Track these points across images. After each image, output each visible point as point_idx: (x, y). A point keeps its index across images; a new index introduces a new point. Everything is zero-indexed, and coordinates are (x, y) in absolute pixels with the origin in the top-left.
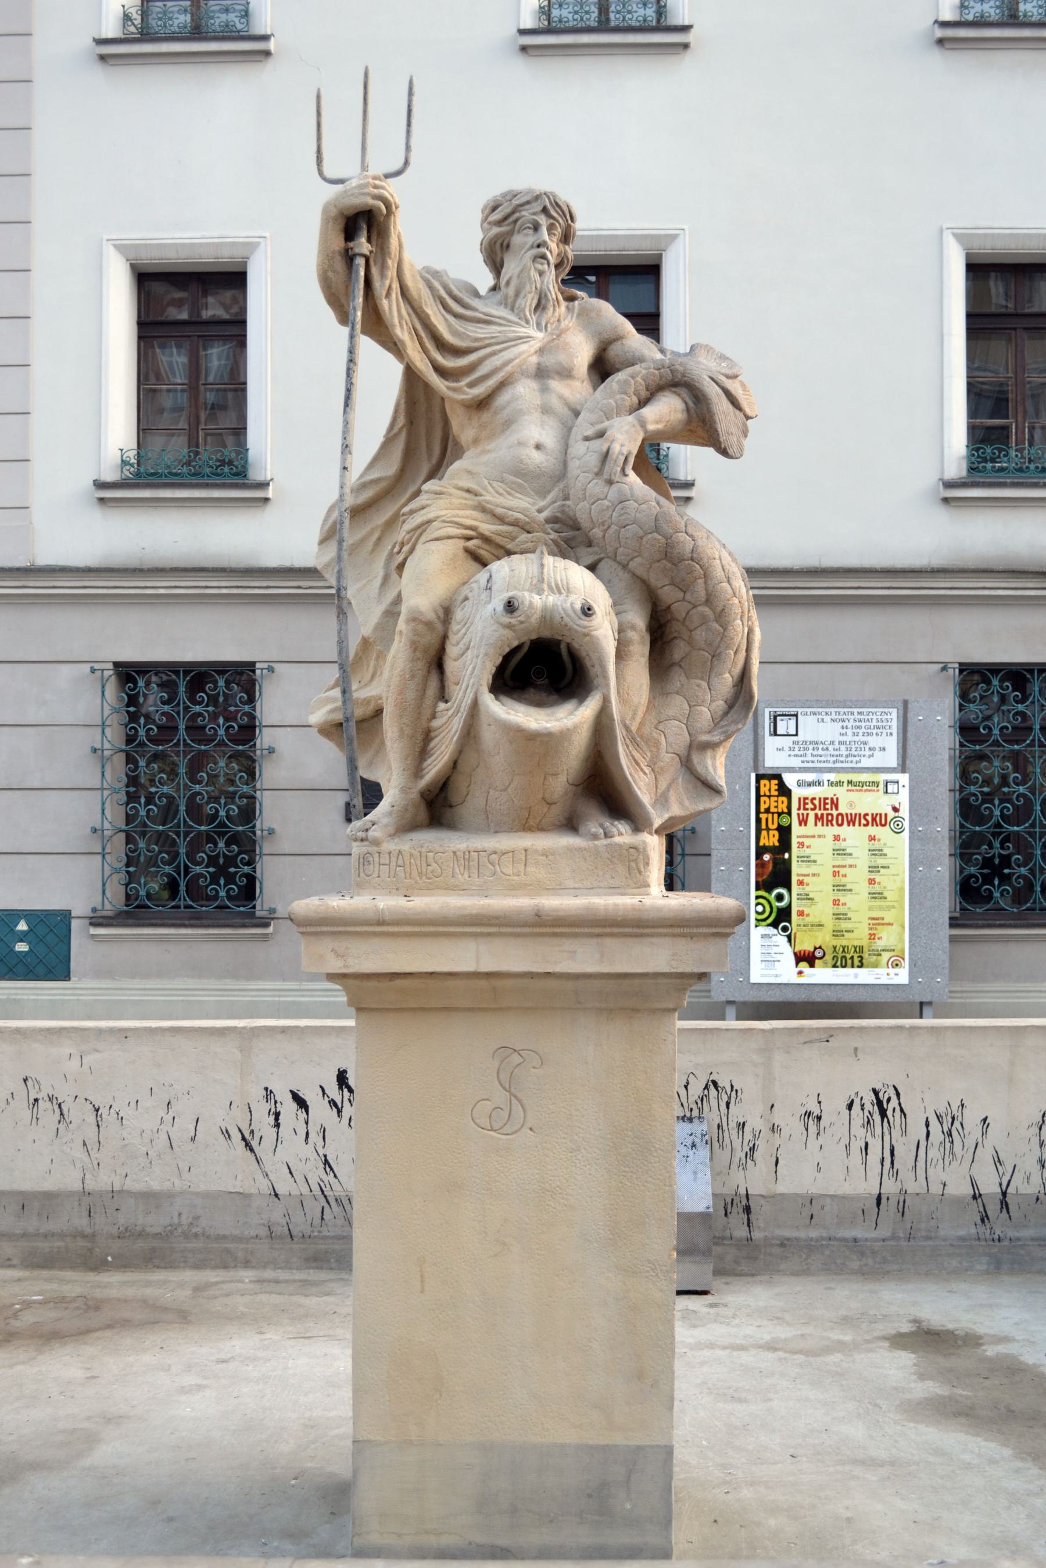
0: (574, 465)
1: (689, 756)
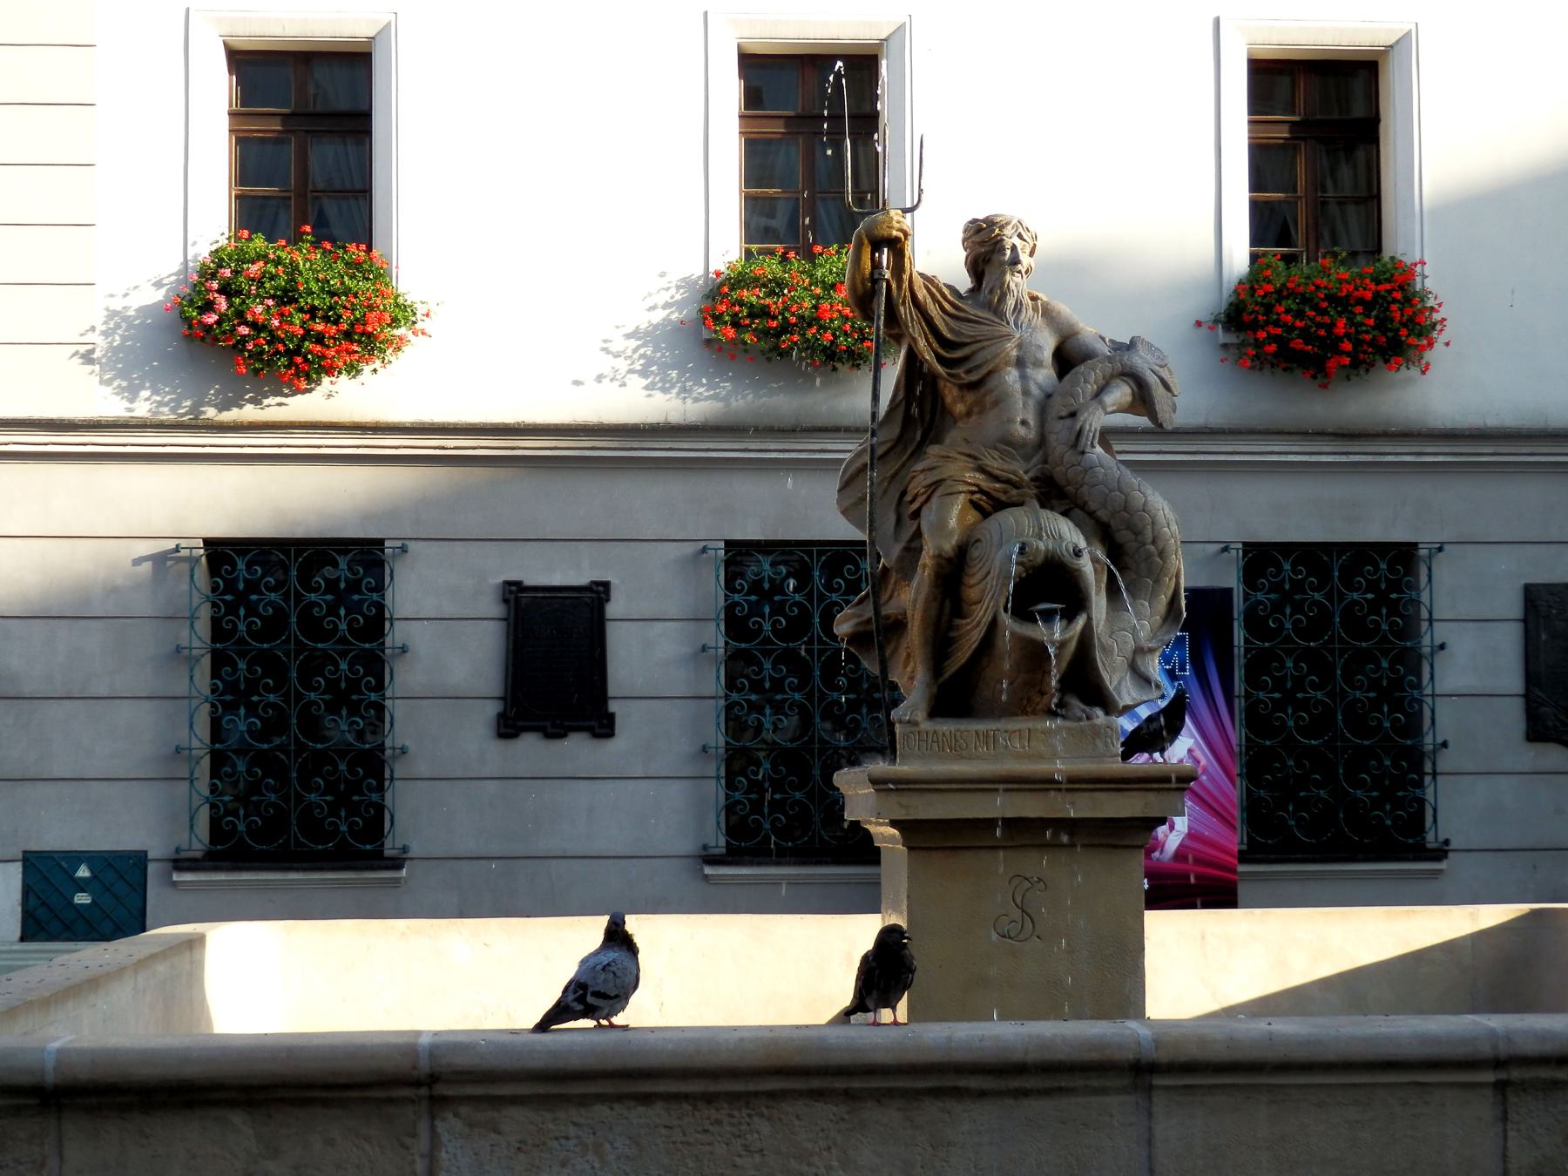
0: (1052, 438)
1: (1134, 660)
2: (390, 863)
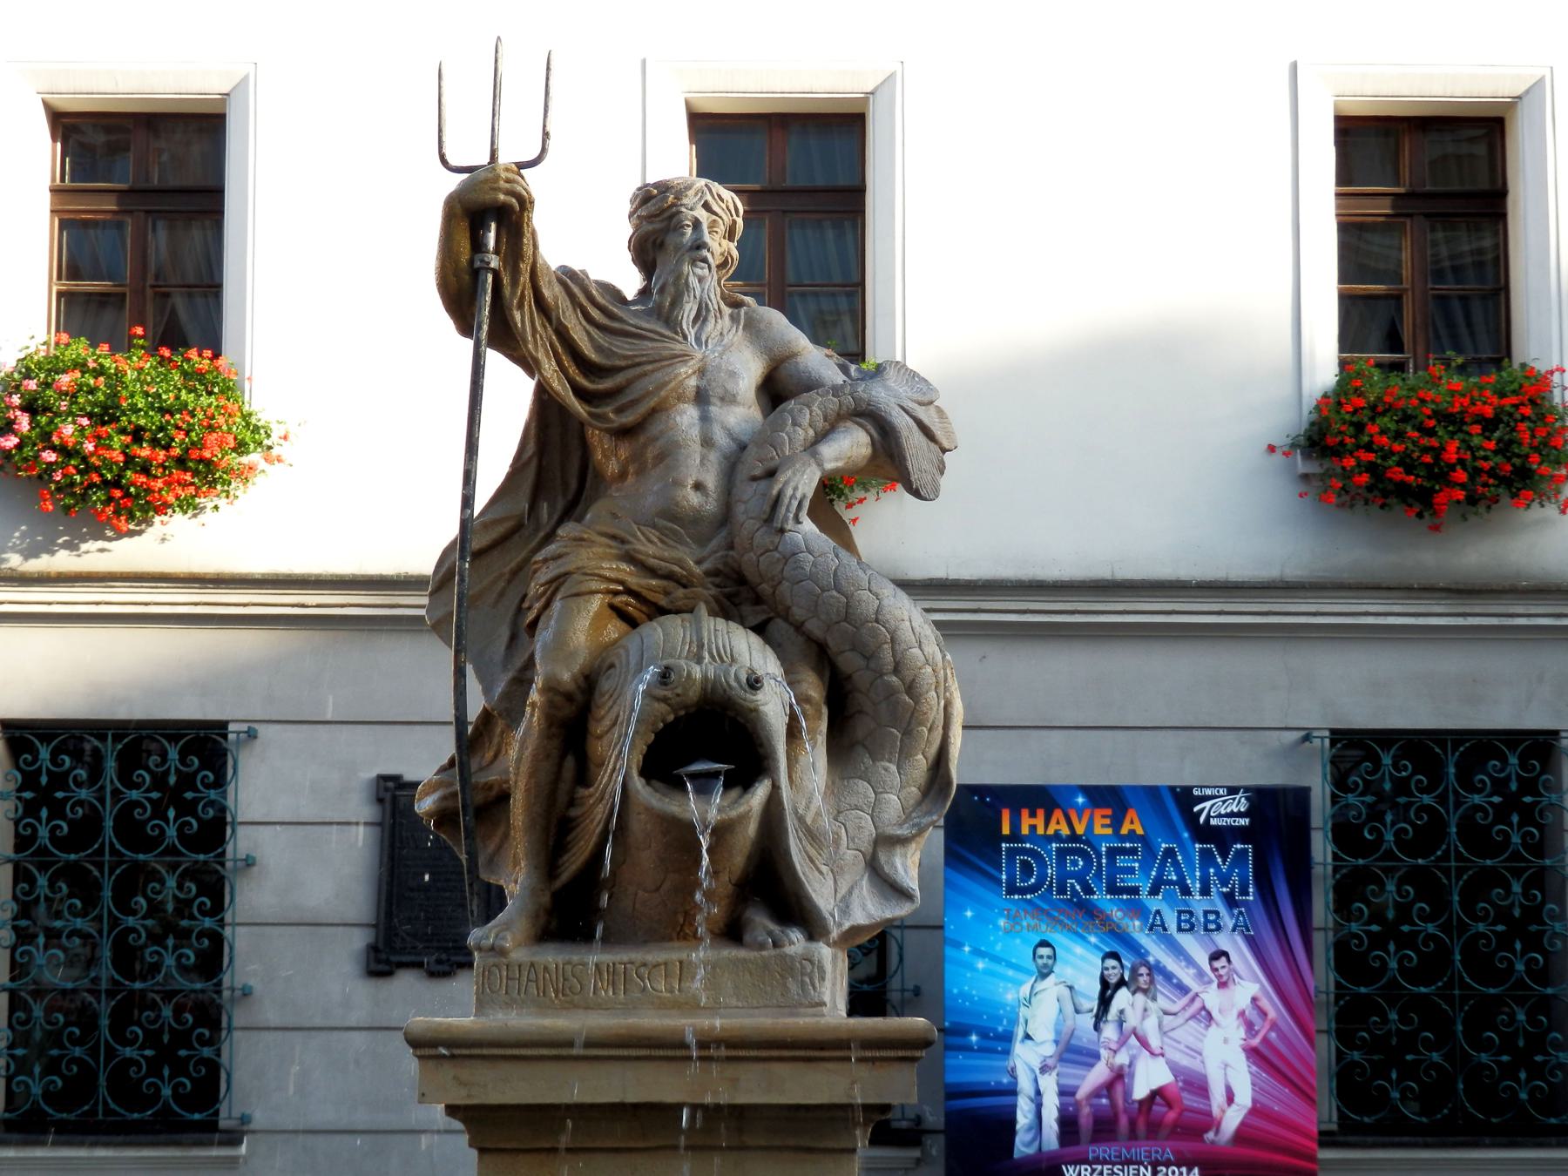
0: (740, 509)
2: (225, 1136)
